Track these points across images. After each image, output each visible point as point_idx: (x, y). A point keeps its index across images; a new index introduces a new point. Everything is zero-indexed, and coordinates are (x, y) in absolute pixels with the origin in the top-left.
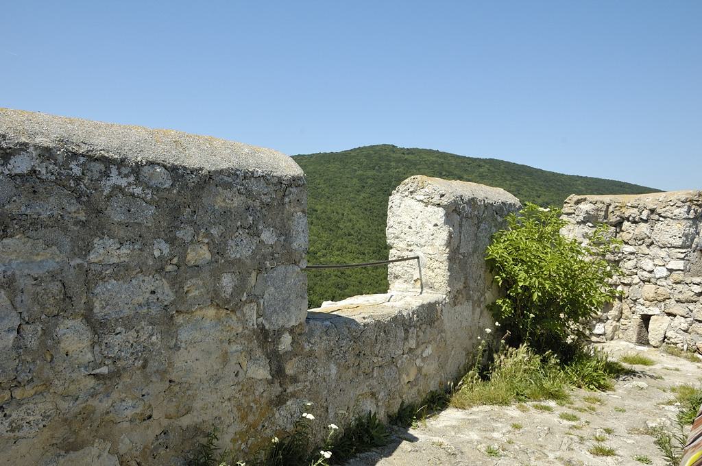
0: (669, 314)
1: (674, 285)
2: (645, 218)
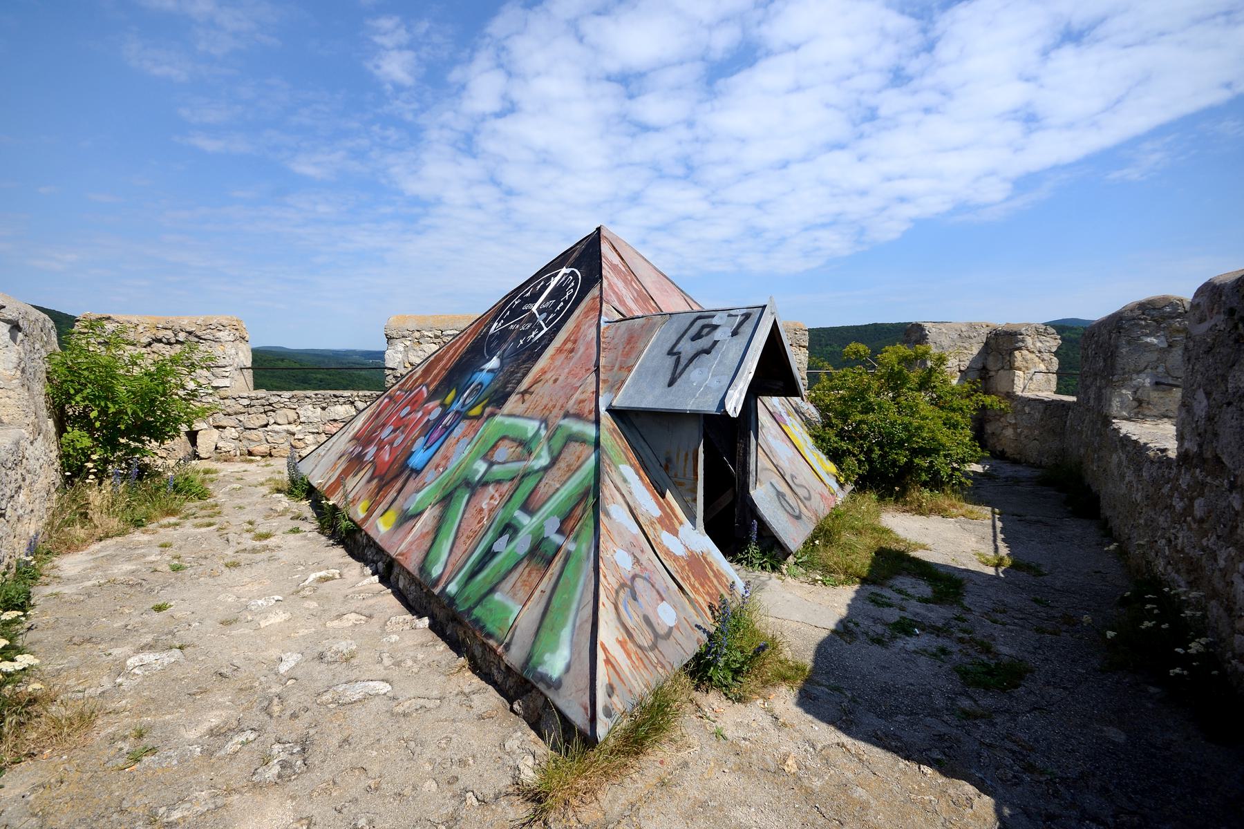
0: (217, 427)
1: (221, 401)
2: (181, 340)
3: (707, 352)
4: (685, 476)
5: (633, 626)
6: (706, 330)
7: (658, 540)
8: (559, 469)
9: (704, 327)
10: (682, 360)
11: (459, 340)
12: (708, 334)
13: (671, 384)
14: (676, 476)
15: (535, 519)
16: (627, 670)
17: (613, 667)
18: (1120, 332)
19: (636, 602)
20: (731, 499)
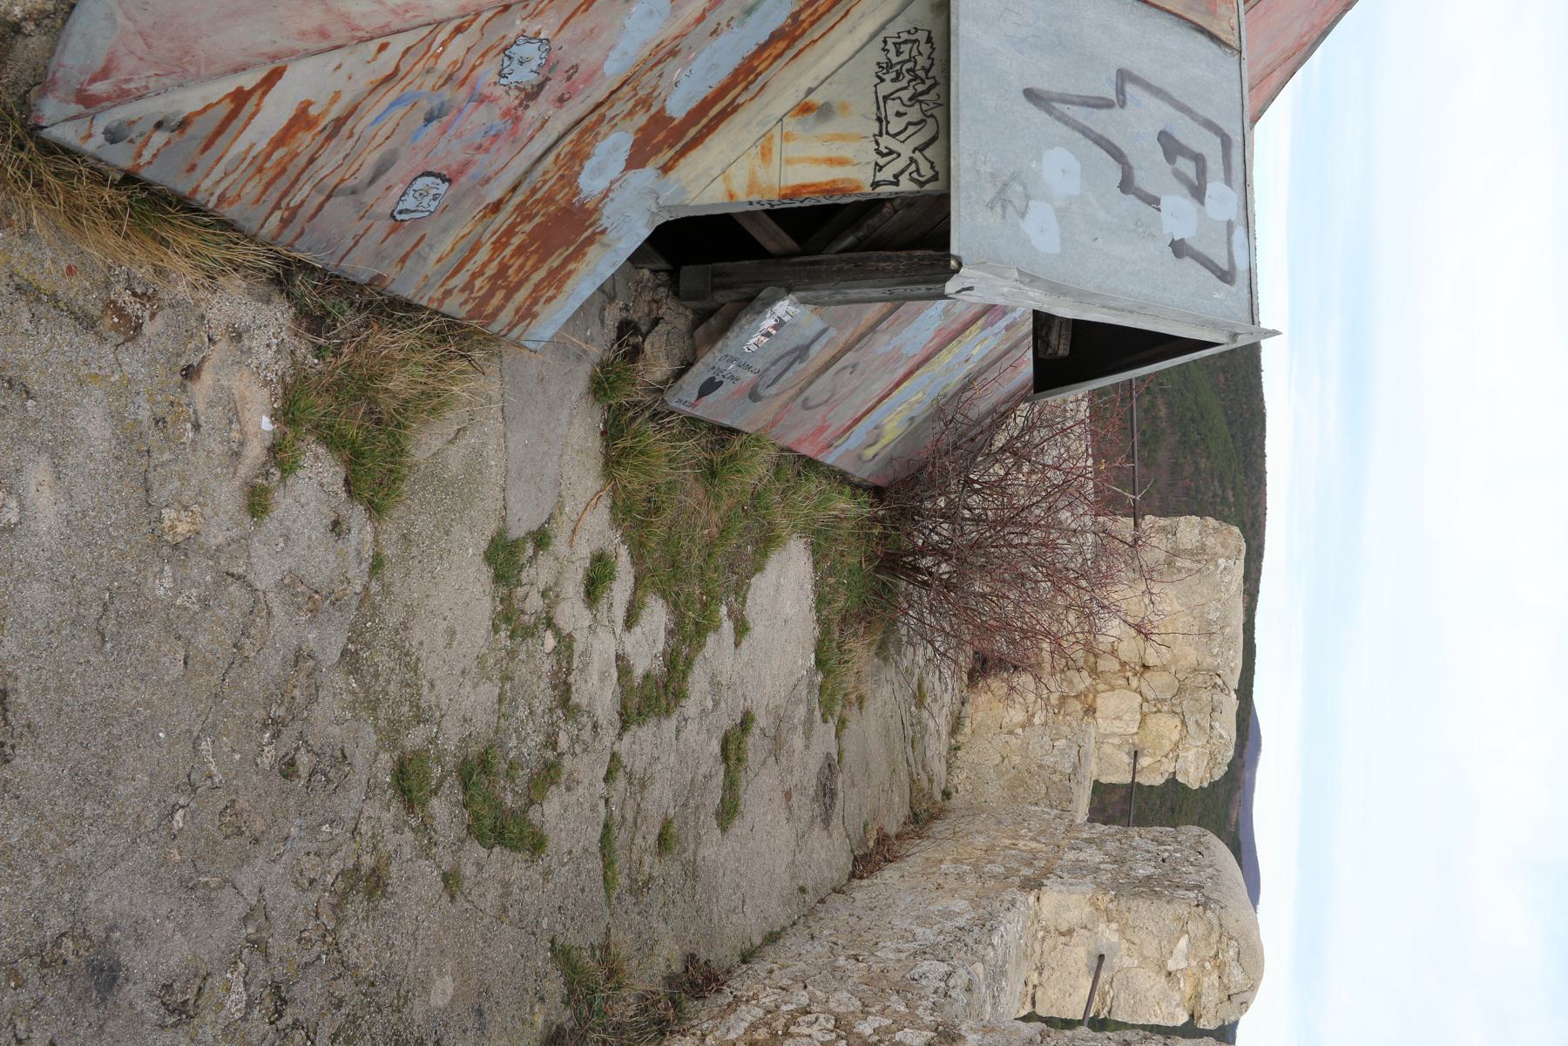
4: (789, 161)
5: (357, 131)
6: (1187, 167)
7: (604, 128)
9: (1199, 160)
10: (1103, 113)
12: (1178, 175)
13: (1031, 95)
14: (786, 137)
16: (240, 146)
17: (233, 115)
18: (1197, 906)
19: (421, 122)
20: (771, 246)
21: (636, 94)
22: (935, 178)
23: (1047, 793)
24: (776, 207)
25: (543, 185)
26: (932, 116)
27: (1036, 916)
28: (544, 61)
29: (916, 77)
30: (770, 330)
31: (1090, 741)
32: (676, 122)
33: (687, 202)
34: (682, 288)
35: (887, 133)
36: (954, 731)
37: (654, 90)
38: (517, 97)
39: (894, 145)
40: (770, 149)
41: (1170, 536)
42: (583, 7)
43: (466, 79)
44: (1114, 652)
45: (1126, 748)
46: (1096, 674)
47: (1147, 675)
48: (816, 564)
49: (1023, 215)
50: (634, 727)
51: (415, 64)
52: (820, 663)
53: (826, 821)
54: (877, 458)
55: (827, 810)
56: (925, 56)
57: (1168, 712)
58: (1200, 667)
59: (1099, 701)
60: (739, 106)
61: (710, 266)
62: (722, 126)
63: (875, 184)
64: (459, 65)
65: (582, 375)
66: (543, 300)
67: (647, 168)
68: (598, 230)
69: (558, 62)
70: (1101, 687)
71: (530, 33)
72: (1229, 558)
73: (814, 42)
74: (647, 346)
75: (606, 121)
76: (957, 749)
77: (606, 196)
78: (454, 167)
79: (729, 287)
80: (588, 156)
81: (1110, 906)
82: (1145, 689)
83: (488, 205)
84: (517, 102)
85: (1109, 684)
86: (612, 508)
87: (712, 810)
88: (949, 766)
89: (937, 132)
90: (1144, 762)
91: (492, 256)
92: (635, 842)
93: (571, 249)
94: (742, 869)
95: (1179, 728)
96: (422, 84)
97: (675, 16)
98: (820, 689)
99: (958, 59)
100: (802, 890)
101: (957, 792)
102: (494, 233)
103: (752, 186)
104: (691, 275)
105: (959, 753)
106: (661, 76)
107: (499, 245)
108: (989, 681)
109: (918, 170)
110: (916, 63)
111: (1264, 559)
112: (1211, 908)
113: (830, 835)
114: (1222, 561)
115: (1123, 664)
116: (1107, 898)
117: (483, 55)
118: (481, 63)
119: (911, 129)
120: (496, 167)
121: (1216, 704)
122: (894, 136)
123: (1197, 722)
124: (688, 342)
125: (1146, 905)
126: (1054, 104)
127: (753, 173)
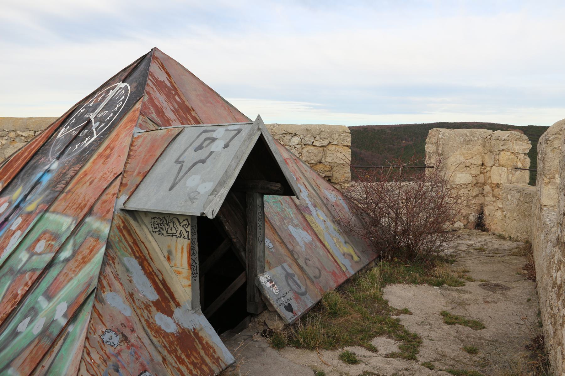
3: (203, 161)
4: (181, 265)
8: (76, 261)
9: (206, 139)
10: (183, 168)
11: (34, 142)
14: (175, 266)
15: (51, 304)
18: (547, 143)
19: (117, 374)
20: (244, 281)
21: (143, 309)
22: (187, 220)
23: (528, 203)
24: (198, 272)
25: (164, 343)
26: (172, 219)
27: (553, 207)
28: (114, 332)
29: (162, 223)
30: (272, 284)
31: (509, 186)
32: (160, 299)
33: (191, 300)
34: (253, 313)
35: (176, 234)
36: (503, 238)
37: (143, 303)
38: (124, 343)
39: (179, 232)
40: (178, 271)
41: (432, 155)
42: (100, 317)
43: (108, 356)
44: (476, 176)
45: (514, 172)
46: (485, 183)
47: (485, 164)
48: (399, 282)
49: (199, 193)
50: (417, 356)
51: (94, 369)
52: (439, 284)
53: (507, 288)
54: (360, 256)
55: (503, 288)
56: (157, 220)
57: (499, 156)
58: (483, 145)
59: (495, 182)
60: (163, 279)
61: (247, 302)
62: (169, 285)
63: (188, 239)
64: (102, 357)
65: (274, 352)
66: (214, 354)
67: (174, 311)
68: (193, 331)
69: (117, 329)
70: (489, 181)
71: (101, 334)
72: (439, 134)
73: (149, 253)
74: (272, 328)
75: (149, 319)
76: (510, 237)
77: (179, 326)
78: (141, 368)
79: (254, 296)
80: (160, 328)
81: (548, 177)
82: (490, 165)
83: (163, 362)
84: (126, 344)
85: (489, 178)
86: (327, 350)
87: (473, 331)
88: (517, 241)
89: (176, 218)
90: (520, 165)
91: (185, 366)
92: (465, 362)
93: (196, 340)
94: (505, 322)
95: (505, 152)
96: (102, 369)
97: (118, 291)
98: (450, 286)
99: (153, 210)
100: (529, 300)
101: (526, 238)
102: (176, 363)
103: (188, 279)
104: (250, 309)
105: (512, 237)
106: (139, 300)
107: (182, 362)
108: (486, 224)
109: (185, 225)
110: (159, 223)
111: (494, 123)
112: (548, 138)
113: (514, 288)
114: (440, 136)
115: (481, 173)
116: (545, 179)
117: (102, 349)
118: (105, 351)
119: (175, 226)
120: (148, 355)
121: (496, 138)
122: (177, 232)
123: (502, 145)
124: (272, 313)
125: (547, 163)
126: (176, 182)
127: (184, 278)
